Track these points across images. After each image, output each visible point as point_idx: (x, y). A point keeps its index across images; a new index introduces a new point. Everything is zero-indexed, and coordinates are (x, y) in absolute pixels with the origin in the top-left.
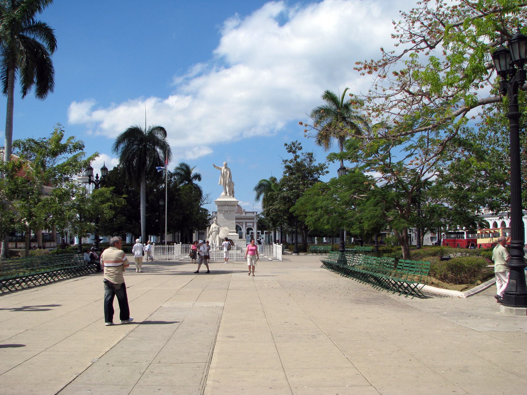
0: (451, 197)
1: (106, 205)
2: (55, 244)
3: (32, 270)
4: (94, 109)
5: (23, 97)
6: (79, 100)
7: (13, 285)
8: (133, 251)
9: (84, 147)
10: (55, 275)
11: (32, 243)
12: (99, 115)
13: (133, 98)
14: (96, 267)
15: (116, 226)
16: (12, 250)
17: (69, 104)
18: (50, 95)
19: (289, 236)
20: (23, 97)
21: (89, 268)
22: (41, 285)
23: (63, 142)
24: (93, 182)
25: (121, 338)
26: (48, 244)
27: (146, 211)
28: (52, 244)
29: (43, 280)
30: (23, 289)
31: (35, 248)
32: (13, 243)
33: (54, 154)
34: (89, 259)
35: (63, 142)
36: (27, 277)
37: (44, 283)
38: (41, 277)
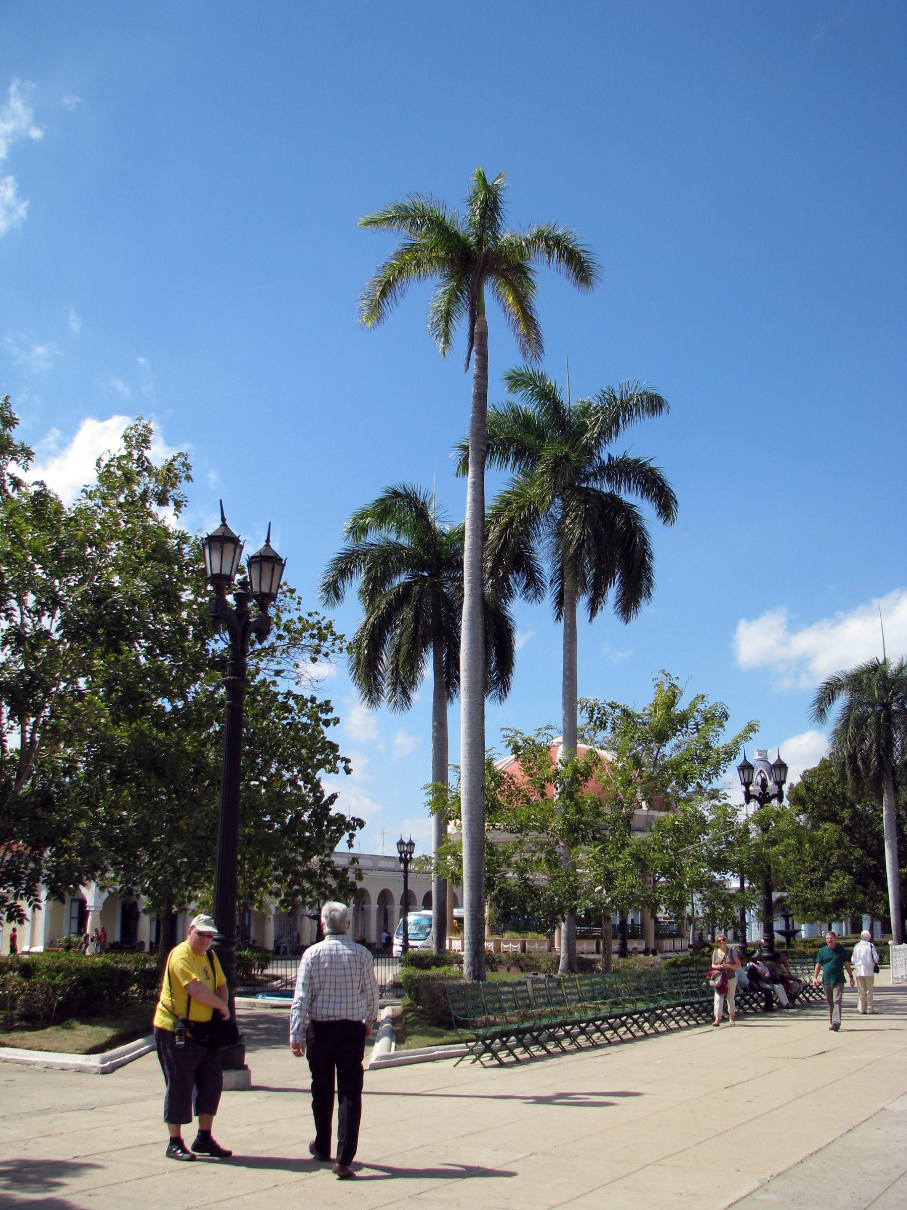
0: (27, 686)
1: (780, 848)
2: (685, 944)
3: (615, 1004)
4: (793, 627)
5: (590, 620)
6: (753, 615)
7: (558, 1041)
8: (852, 959)
9: (726, 716)
10: (659, 1017)
11: (578, 942)
12: (805, 641)
13: (881, 593)
14: (763, 1000)
15: (829, 899)
16: (583, 956)
17: (734, 627)
18: (646, 609)
19: (491, 907)
20: (590, 620)
21: (747, 1002)
22: (622, 1041)
23: (682, 706)
24: (754, 797)
25: (743, 1194)
26: (667, 944)
27: (899, 860)
28: (678, 944)
29: (629, 1029)
30: (580, 1049)
31: (636, 951)
32: (590, 941)
33: (662, 737)
34: (747, 981)
35: (682, 706)
36: (604, 1019)
37: (629, 1036)
38: (623, 1024)
